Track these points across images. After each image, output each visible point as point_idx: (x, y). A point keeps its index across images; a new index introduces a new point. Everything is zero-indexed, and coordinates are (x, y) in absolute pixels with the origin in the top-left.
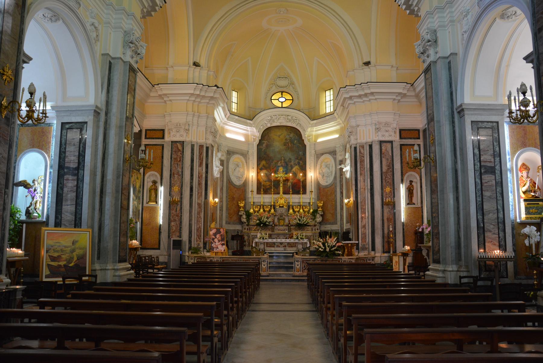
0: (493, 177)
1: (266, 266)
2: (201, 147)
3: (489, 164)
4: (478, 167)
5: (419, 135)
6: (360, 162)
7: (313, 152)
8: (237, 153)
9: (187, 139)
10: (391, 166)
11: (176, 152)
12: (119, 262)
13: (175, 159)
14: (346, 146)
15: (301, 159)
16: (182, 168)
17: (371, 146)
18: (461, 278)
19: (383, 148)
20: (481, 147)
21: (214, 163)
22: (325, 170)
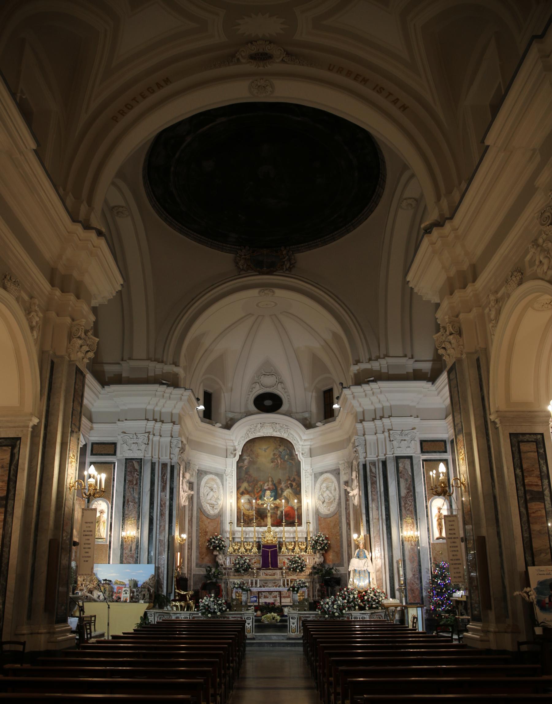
0: (542, 505)
1: (251, 624)
2: (164, 465)
3: (536, 489)
4: (521, 493)
5: (446, 447)
6: (372, 484)
7: (310, 471)
8: (211, 473)
9: (148, 456)
10: (412, 488)
11: (131, 472)
12: (56, 623)
13: (130, 481)
14: (352, 463)
15: (294, 480)
16: (139, 493)
17: (384, 463)
18: (520, 644)
19: (400, 465)
20: (525, 466)
21: (181, 486)
22: (327, 494)
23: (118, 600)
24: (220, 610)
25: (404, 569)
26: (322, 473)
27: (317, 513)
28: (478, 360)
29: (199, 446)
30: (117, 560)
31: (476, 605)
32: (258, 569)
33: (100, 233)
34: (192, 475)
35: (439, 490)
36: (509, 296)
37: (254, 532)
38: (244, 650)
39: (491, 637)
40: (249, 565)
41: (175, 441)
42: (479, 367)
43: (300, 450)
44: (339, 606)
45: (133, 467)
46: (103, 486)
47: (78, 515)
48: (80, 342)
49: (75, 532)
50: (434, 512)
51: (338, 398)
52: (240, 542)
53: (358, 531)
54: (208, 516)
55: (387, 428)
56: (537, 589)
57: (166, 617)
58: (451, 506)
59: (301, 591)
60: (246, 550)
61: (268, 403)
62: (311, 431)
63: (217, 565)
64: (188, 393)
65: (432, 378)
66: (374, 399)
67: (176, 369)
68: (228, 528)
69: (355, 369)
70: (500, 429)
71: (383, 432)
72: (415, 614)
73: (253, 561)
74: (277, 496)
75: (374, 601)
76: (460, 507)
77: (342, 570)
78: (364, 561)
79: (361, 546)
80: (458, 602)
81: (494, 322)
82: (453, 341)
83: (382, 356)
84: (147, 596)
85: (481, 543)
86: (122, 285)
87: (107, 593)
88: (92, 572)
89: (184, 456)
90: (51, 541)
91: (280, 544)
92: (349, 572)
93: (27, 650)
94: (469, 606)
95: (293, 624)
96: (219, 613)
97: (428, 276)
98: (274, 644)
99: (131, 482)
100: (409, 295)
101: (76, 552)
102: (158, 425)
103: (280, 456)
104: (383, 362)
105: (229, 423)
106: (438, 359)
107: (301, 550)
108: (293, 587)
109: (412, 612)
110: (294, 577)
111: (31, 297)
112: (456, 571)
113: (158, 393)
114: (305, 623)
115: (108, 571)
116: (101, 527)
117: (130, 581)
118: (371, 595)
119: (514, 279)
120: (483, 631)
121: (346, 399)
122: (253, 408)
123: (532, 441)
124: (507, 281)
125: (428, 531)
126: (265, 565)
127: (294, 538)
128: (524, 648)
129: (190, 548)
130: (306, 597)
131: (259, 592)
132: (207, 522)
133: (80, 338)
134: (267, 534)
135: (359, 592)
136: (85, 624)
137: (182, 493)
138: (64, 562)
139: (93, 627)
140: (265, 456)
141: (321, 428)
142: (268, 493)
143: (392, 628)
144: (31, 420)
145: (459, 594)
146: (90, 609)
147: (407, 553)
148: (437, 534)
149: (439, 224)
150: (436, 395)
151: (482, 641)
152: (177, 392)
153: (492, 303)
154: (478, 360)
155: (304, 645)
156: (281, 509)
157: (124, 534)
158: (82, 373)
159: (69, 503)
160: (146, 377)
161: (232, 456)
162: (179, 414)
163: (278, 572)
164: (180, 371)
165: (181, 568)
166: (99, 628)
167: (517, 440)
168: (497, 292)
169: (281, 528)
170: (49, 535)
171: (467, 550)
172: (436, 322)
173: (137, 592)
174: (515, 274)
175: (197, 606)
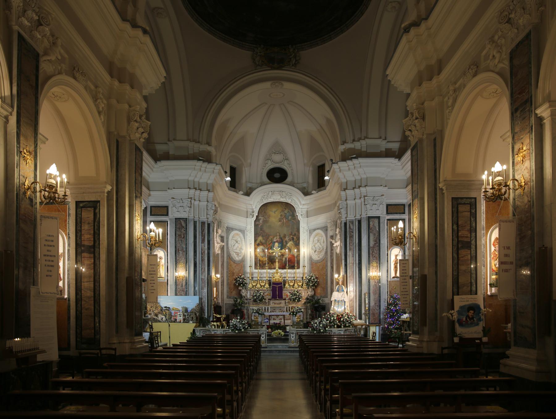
2: (203, 223)
3: (466, 240)
5: (404, 210)
6: (350, 237)
7: (306, 228)
8: (236, 230)
9: (191, 217)
10: (378, 241)
11: (179, 228)
13: (179, 235)
14: (337, 222)
15: (295, 235)
17: (360, 222)
18: (443, 348)
19: (371, 223)
20: (460, 223)
23: (175, 321)
24: (244, 328)
25: (369, 300)
26: (315, 230)
27: (311, 259)
28: (435, 139)
29: (228, 209)
30: (174, 295)
31: (416, 324)
32: (269, 299)
33: (145, 32)
34: (223, 231)
35: (398, 241)
36: (465, 86)
37: (267, 273)
38: (260, 355)
39: (424, 344)
40: (263, 297)
41: (210, 205)
42: (435, 145)
43: (300, 212)
44: (323, 325)
45: (181, 225)
46: (161, 238)
47: (144, 260)
48: (137, 125)
49: (143, 274)
50: (393, 258)
51: (328, 171)
52: (257, 281)
53: (339, 273)
54: (234, 262)
55: (363, 195)
56: (458, 311)
57: (207, 333)
58: (404, 254)
59: (298, 315)
60: (261, 286)
61: (277, 175)
62: (308, 197)
63: (241, 297)
64: (219, 167)
65: (399, 155)
66: (355, 172)
67: (209, 148)
68: (248, 270)
69: (342, 148)
70: (445, 194)
71: (360, 198)
72: (374, 331)
73: (266, 294)
74: (282, 247)
75: (348, 321)
76: (411, 254)
77: (326, 300)
78: (342, 293)
79: (340, 283)
80: (404, 322)
81: (450, 108)
82: (417, 125)
83: (363, 138)
84: (195, 318)
85: (424, 278)
86: (165, 77)
87: (167, 316)
88: (157, 300)
89: (217, 216)
90: (127, 278)
91: (285, 282)
92: (331, 302)
93: (118, 354)
94: (411, 325)
95: (293, 337)
96: (243, 330)
97: (402, 72)
98: (280, 351)
99: (180, 235)
100: (387, 85)
101: (145, 287)
102: (198, 192)
103: (285, 216)
104: (363, 142)
105: (249, 191)
106: (405, 140)
107: (299, 286)
108: (293, 312)
109: (373, 329)
110: (294, 305)
111: (96, 87)
112: (404, 299)
113: (196, 167)
114: (300, 337)
115: (168, 301)
116: (161, 270)
117: (183, 308)
118: (346, 317)
119: (470, 71)
120: (419, 341)
121: (334, 172)
122: (266, 179)
123: (468, 204)
124: (464, 74)
125: (387, 272)
126: (274, 297)
127: (294, 277)
128: (446, 351)
129: (223, 285)
130: (302, 319)
131: (270, 316)
132: (234, 265)
133: (136, 121)
134: (275, 275)
135: (338, 316)
136: (154, 337)
137: (216, 244)
138: (137, 294)
139: (159, 339)
140: (274, 216)
141: (316, 195)
142: (277, 244)
143: (359, 339)
144: (105, 187)
145: (405, 316)
146: (157, 327)
147: (371, 288)
148: (393, 275)
149: (416, 24)
150: (401, 169)
151: (417, 347)
152: (211, 166)
153: (451, 92)
154: (435, 139)
155: (300, 352)
156: (285, 256)
157: (176, 274)
158: (140, 150)
159: (138, 251)
160: (187, 154)
161: (251, 216)
162: (212, 184)
163: (283, 301)
164: (212, 149)
165: (217, 299)
166: (164, 340)
167: (456, 202)
168: (455, 83)
169: (285, 270)
170: (125, 274)
171: (413, 286)
172: (406, 109)
173: (188, 316)
174: (472, 67)
175: (228, 325)
